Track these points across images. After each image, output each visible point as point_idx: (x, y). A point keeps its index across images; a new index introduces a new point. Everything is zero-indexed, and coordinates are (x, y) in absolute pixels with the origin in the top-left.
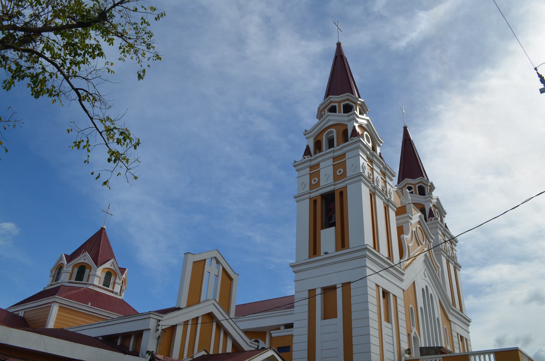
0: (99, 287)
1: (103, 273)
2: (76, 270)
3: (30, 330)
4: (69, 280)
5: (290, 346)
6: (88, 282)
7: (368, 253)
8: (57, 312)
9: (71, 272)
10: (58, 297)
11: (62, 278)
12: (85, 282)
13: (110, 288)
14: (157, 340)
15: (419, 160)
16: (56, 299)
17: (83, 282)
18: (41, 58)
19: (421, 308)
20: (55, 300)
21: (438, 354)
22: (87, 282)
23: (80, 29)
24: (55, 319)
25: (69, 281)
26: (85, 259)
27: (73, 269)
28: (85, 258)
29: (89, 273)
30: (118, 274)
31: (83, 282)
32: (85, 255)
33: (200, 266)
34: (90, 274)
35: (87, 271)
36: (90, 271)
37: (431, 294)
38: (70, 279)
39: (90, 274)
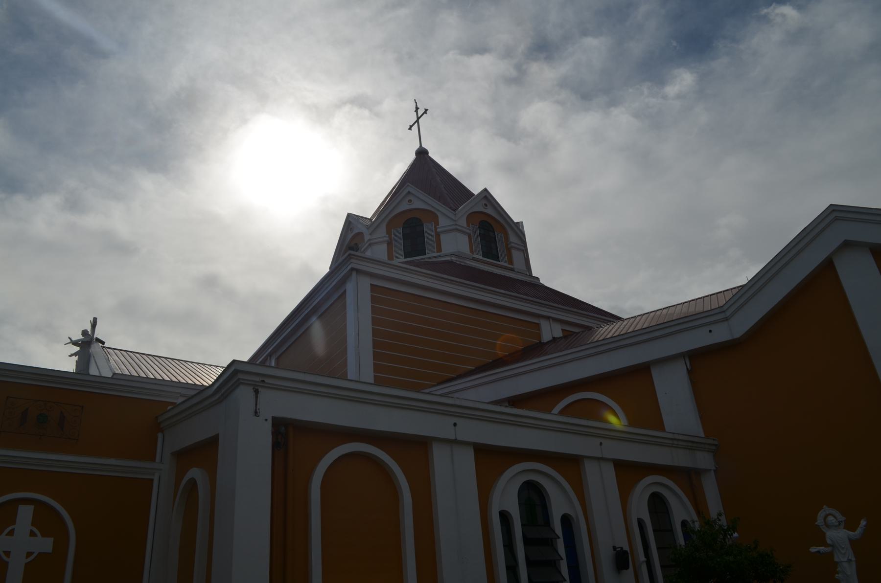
2: (398, 233)
5: (10, 552)
6: (441, 253)
7: (240, 376)
8: (369, 304)
9: (387, 238)
15: (221, 380)
18: (75, 354)
19: (641, 523)
22: (438, 252)
24: (371, 313)
27: (389, 232)
28: (410, 197)
29: (436, 229)
30: (438, 210)
31: (427, 256)
32: (409, 193)
34: (438, 230)
35: (428, 228)
36: (437, 223)
37: (566, 520)
39: (438, 230)
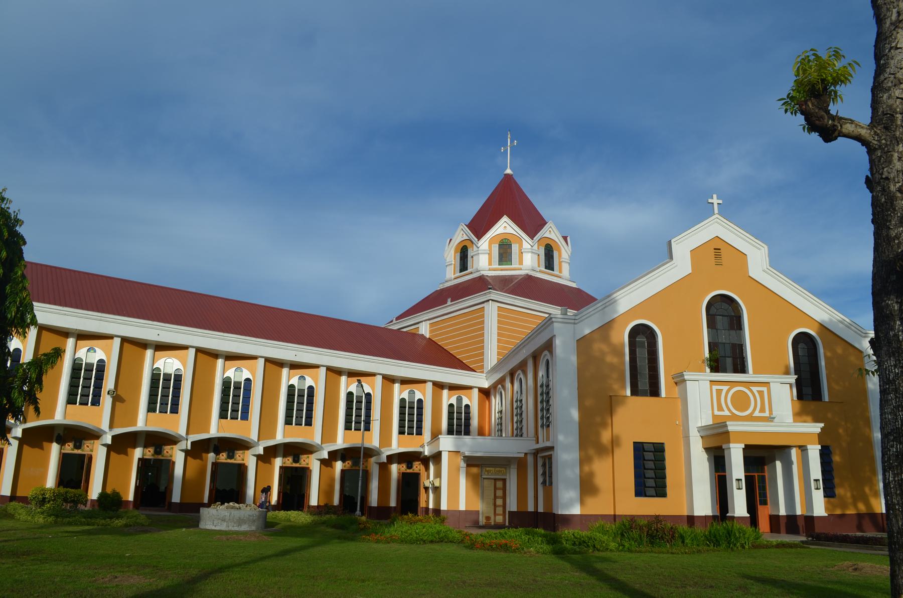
0: (541, 272)
1: (540, 247)
3: (882, 423)
4: (489, 265)
10: (688, 373)
11: (453, 252)
12: (517, 266)
13: (556, 272)
14: (530, 268)
16: (492, 295)
17: (513, 266)
20: (493, 297)
21: (725, 371)
23: (682, 428)
25: (490, 267)
26: (505, 227)
31: (513, 266)
33: (719, 249)
35: (515, 248)
38: (490, 264)
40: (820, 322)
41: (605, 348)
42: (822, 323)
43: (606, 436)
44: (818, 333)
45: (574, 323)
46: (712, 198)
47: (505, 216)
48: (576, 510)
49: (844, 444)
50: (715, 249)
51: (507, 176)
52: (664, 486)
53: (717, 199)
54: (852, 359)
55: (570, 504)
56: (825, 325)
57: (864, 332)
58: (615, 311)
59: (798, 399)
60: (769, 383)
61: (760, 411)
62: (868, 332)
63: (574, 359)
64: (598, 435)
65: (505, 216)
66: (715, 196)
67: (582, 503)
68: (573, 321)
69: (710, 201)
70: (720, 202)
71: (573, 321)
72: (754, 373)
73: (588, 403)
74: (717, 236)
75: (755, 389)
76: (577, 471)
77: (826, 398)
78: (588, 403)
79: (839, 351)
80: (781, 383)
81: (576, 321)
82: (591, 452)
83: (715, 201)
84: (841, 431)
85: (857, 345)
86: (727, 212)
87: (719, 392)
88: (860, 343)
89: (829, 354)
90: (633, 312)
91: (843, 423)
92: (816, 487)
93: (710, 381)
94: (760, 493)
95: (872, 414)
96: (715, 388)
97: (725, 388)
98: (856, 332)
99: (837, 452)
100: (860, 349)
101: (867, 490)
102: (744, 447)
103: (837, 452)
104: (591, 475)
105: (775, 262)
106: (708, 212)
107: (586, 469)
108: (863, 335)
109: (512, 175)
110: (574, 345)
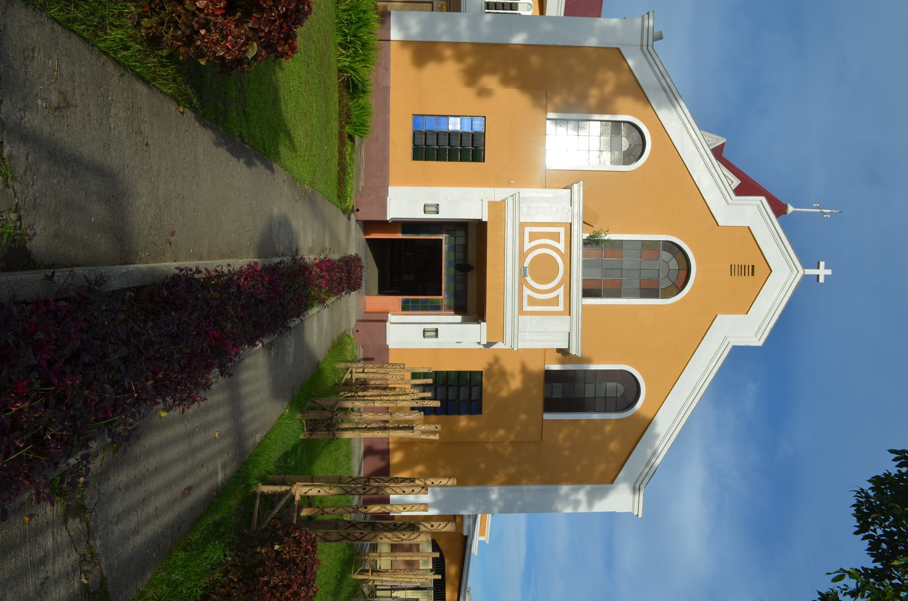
40: (654, 419)
41: (609, 88)
42: (653, 422)
43: (490, 81)
44: (636, 415)
45: (642, 46)
46: (826, 268)
47: (740, 182)
48: (395, 34)
49: (483, 436)
50: (753, 267)
51: (786, 207)
52: (427, 158)
53: (825, 268)
54: (602, 467)
55: (403, 27)
56: (650, 427)
57: (642, 487)
58: (659, 106)
59: (546, 370)
60: (570, 315)
61: (529, 297)
62: (642, 493)
63: (593, 42)
64: (493, 71)
65: (740, 182)
66: (829, 272)
67: (404, 43)
68: (645, 43)
69: (822, 264)
70: (822, 280)
71: (645, 43)
72: (584, 307)
73: (535, 60)
74: (771, 271)
75: (561, 291)
76: (445, 38)
77: (547, 416)
78: (535, 60)
79: (613, 446)
80: (569, 333)
81: (645, 48)
82: (470, 60)
83: (823, 272)
84: (501, 432)
85: (621, 474)
86: (807, 285)
87: (556, 237)
88: (625, 480)
89: (608, 428)
90: (660, 130)
91: (512, 437)
92: (425, 330)
93: (571, 224)
94: (417, 301)
95: (525, 487)
96: (562, 230)
97: (561, 246)
98: (641, 474)
99: (473, 424)
100: (615, 482)
101: (420, 468)
102: (483, 220)
103: (473, 424)
104: (440, 59)
105: (738, 354)
106: (807, 258)
107: (448, 52)
108: (637, 486)
109: (786, 213)
110: (612, 43)
